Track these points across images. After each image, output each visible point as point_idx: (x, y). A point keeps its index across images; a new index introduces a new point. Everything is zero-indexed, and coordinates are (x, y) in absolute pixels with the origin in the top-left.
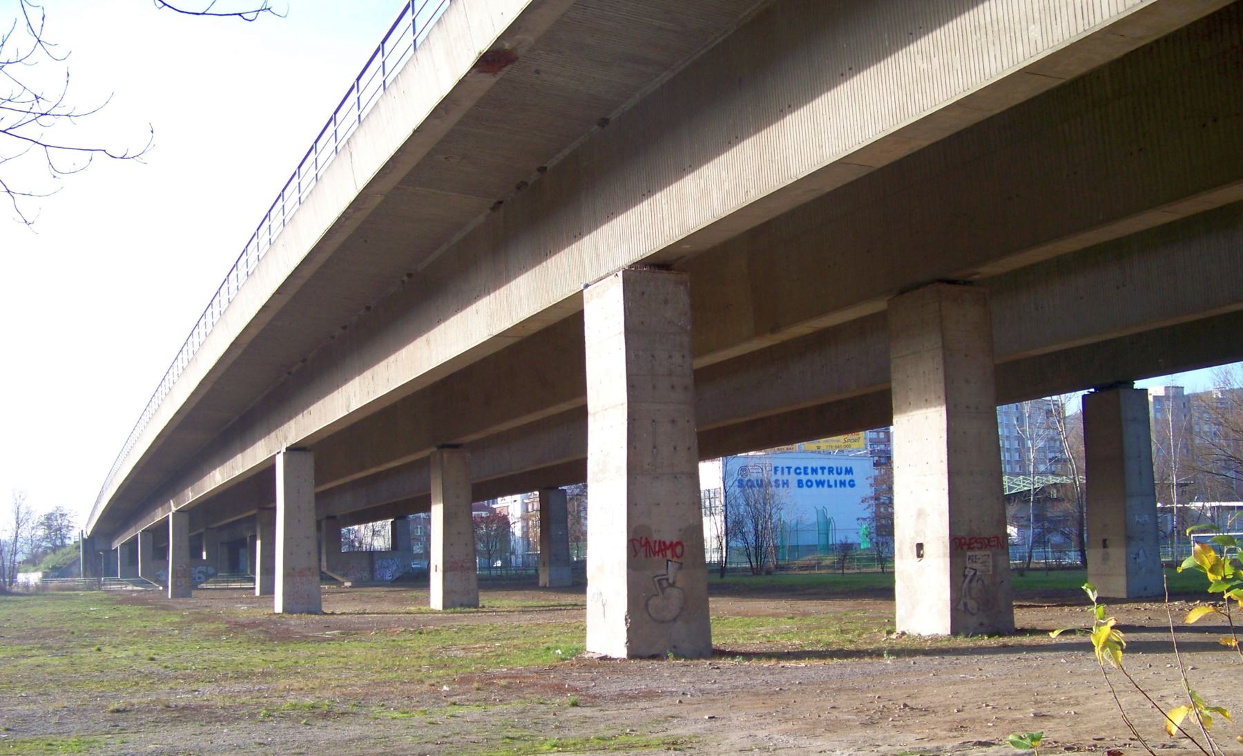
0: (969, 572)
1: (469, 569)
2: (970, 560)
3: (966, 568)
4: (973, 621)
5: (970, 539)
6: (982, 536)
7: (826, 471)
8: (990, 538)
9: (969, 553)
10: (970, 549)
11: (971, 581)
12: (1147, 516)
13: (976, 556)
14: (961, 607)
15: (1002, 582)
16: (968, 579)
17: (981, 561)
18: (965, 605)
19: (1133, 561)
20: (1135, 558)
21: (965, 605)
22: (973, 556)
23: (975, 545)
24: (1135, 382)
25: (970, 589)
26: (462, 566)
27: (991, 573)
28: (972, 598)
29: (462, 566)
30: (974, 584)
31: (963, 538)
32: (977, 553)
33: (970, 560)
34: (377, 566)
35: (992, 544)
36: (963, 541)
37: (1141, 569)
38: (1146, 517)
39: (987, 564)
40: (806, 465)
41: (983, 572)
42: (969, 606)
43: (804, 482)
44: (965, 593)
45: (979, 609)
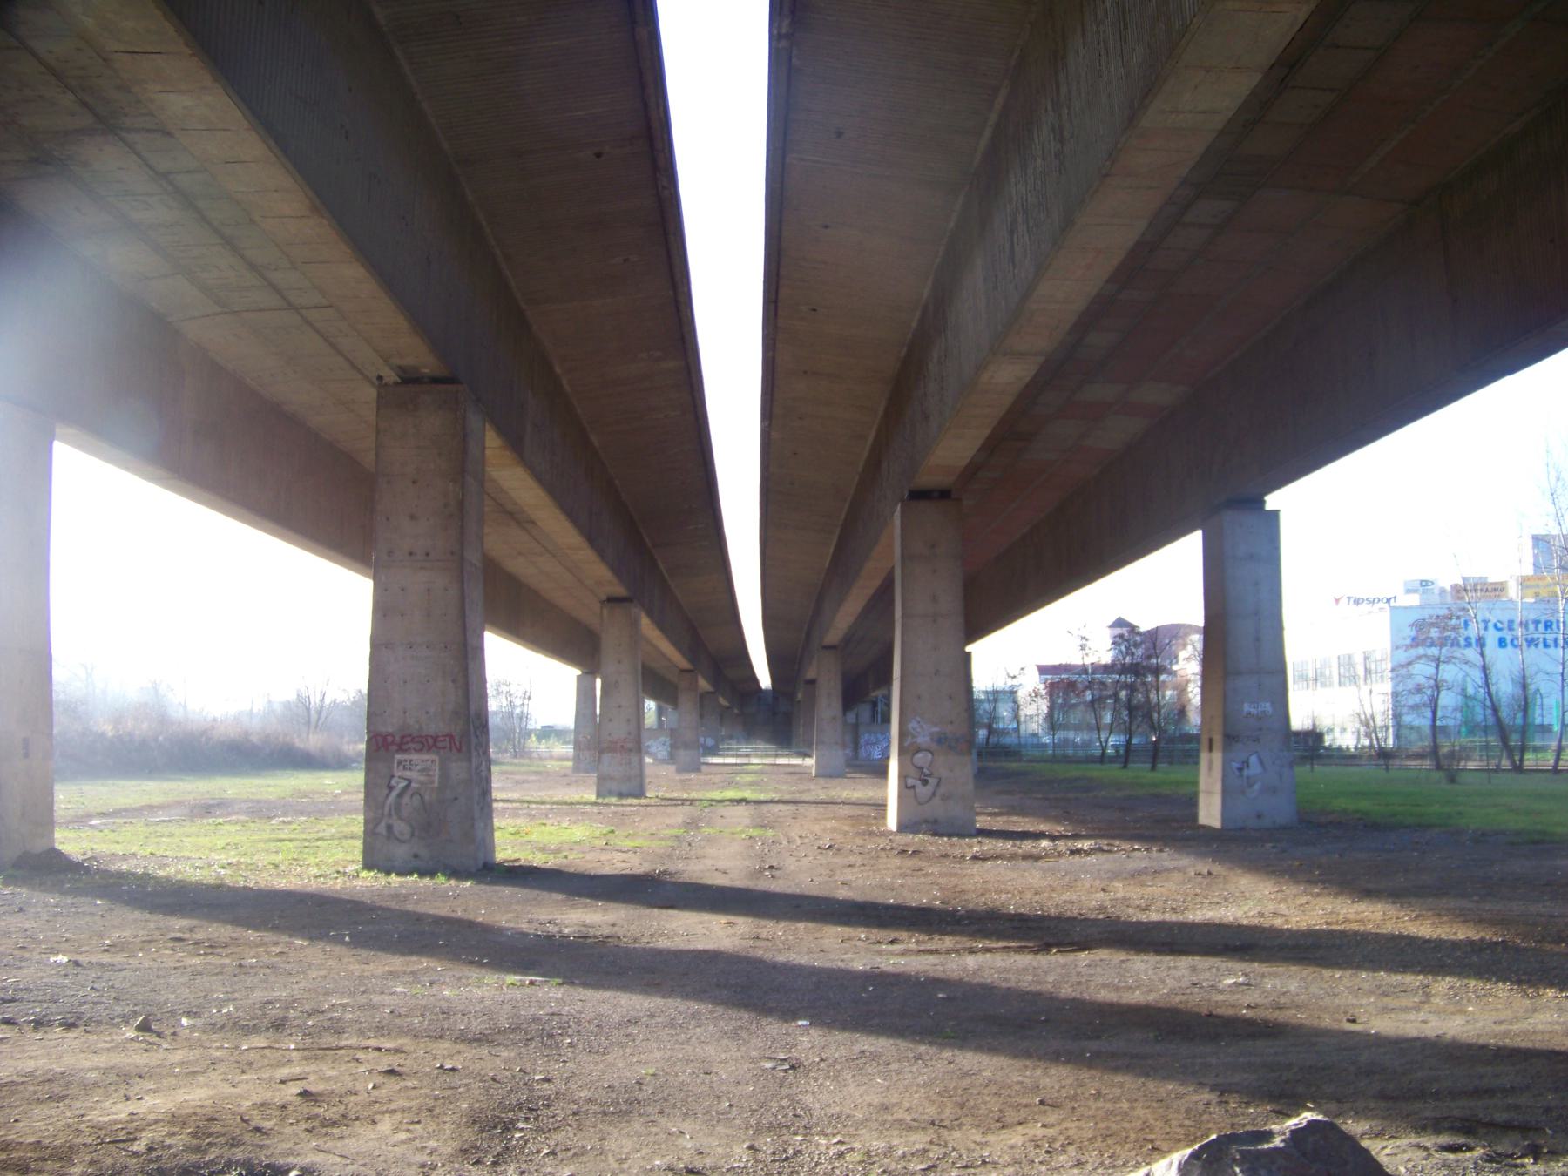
0: (398, 783)
1: (631, 750)
2: (401, 767)
3: (393, 776)
4: (401, 852)
5: (403, 737)
6: (424, 734)
7: (1541, 627)
8: (437, 737)
9: (398, 757)
10: (401, 749)
11: (400, 795)
12: (1268, 705)
13: (411, 761)
14: (382, 829)
15: (456, 799)
16: (394, 794)
17: (419, 767)
18: (389, 828)
19: (1237, 773)
20: (1240, 770)
21: (389, 828)
22: (405, 761)
23: (412, 745)
24: (1272, 501)
25: (398, 807)
26: (622, 747)
27: (436, 784)
28: (400, 818)
29: (622, 747)
30: (406, 799)
31: (391, 735)
32: (414, 757)
33: (401, 767)
34: (862, 741)
35: (440, 745)
36: (390, 739)
37: (1250, 786)
38: (1267, 706)
39: (431, 773)
40: (1512, 618)
41: (422, 783)
42: (396, 829)
43: (1508, 641)
44: (390, 810)
45: (412, 835)
